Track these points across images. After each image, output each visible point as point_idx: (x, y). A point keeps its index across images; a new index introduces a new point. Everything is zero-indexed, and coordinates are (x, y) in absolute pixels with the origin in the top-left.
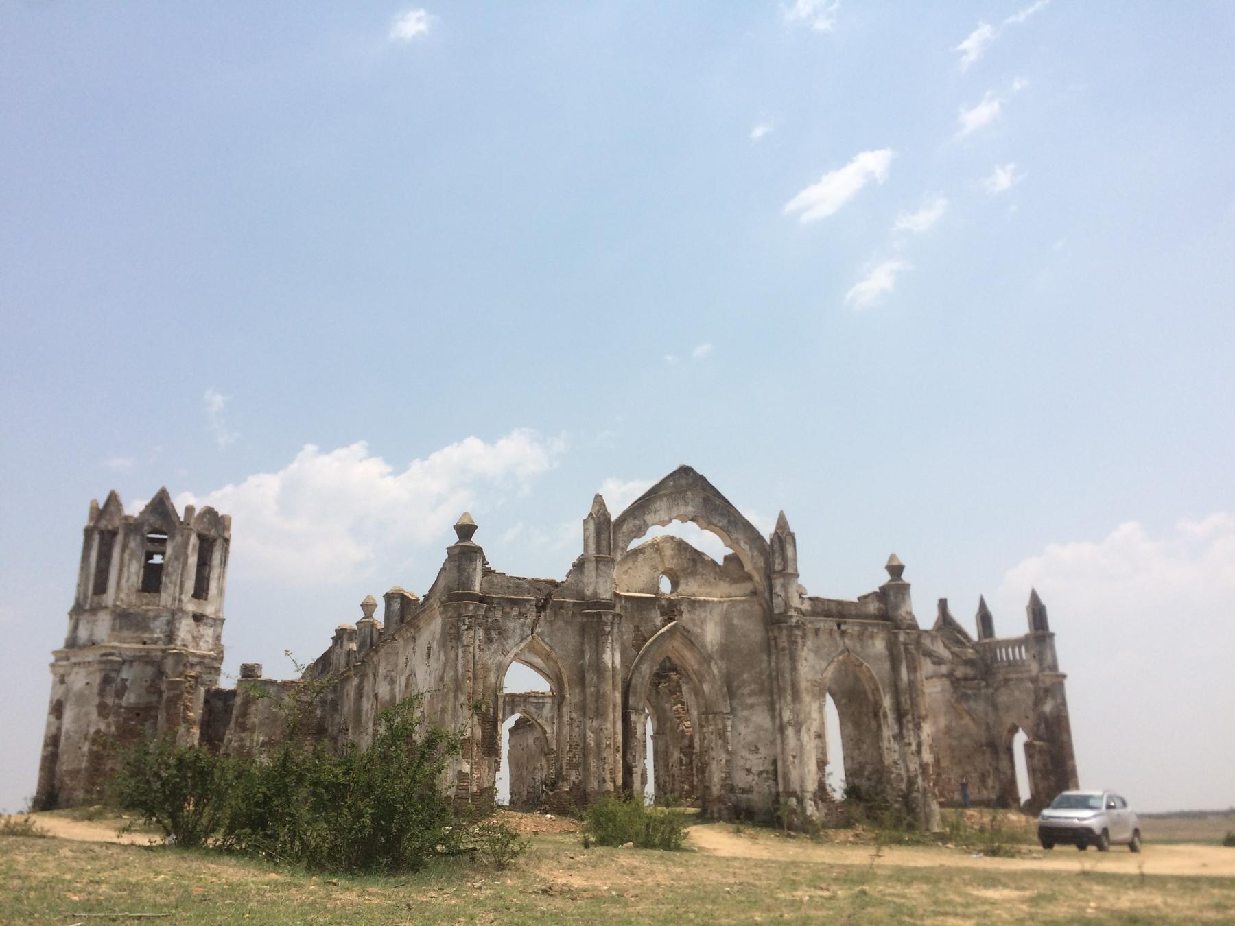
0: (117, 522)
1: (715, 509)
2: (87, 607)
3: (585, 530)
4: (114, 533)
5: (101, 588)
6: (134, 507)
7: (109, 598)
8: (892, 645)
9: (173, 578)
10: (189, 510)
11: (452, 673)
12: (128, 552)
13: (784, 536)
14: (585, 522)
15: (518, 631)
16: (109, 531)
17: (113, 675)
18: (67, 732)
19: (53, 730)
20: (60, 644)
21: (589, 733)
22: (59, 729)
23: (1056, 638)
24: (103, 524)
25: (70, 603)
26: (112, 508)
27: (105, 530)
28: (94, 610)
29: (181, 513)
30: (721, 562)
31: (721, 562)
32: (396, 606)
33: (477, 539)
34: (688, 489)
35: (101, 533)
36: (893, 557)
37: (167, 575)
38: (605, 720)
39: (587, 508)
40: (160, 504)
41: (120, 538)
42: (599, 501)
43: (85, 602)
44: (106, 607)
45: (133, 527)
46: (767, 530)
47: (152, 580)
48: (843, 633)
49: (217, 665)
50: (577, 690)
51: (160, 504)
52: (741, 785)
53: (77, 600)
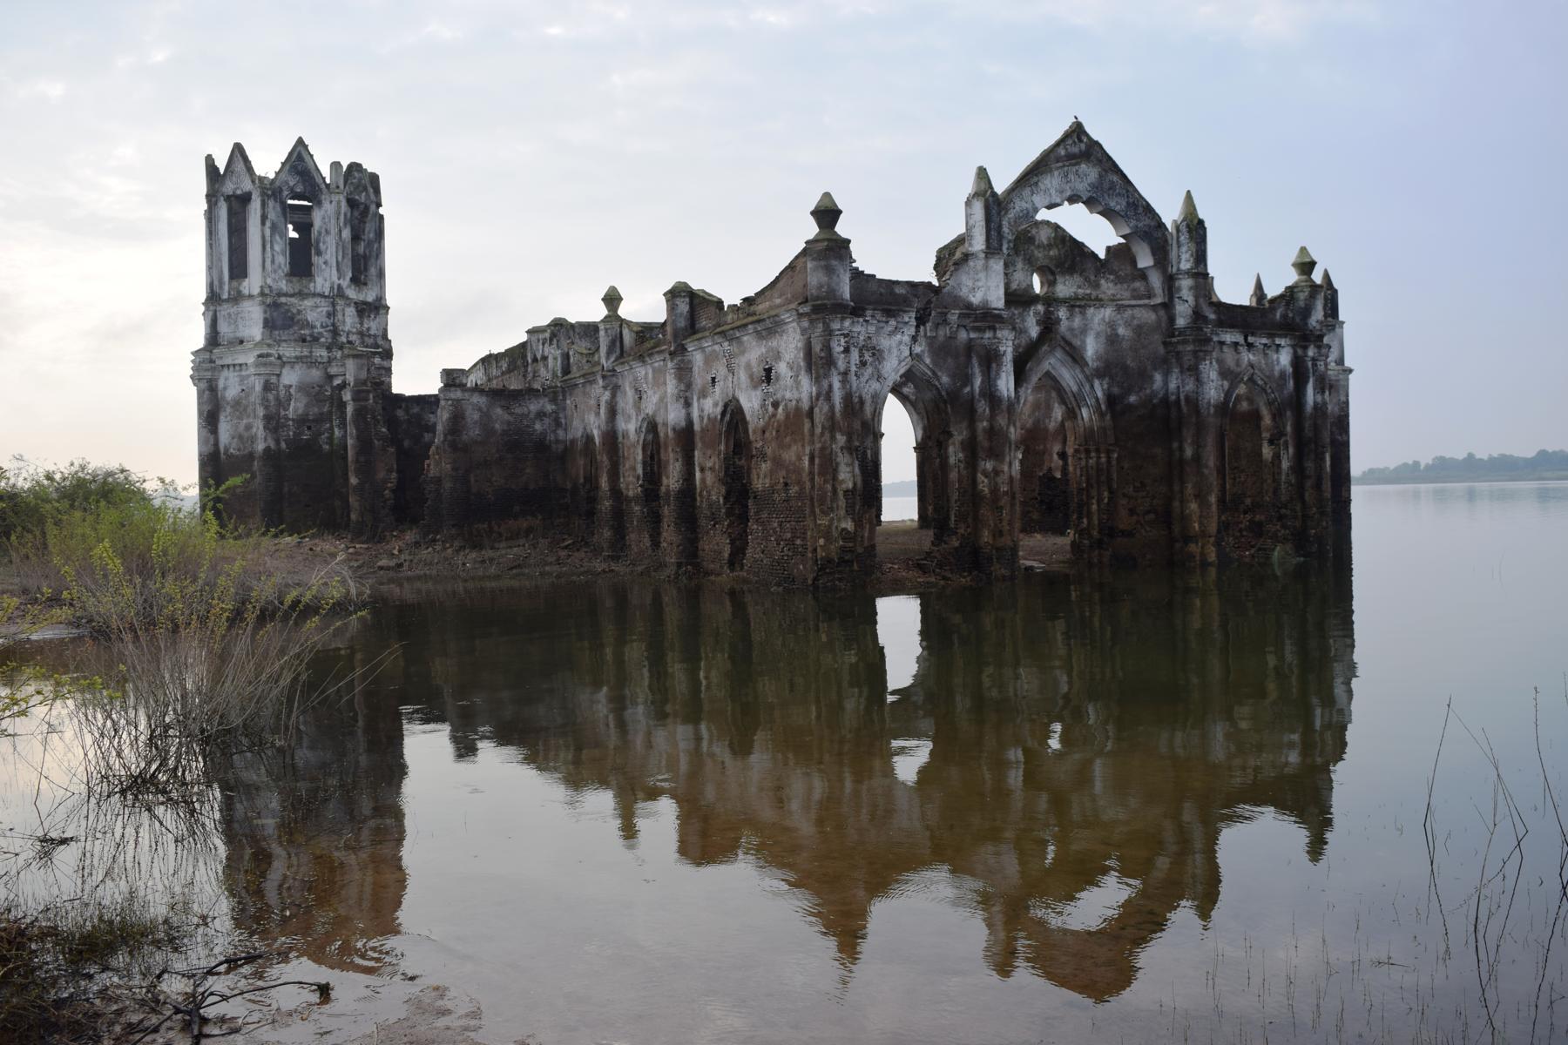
0: (247, 186)
1: (1111, 190)
2: (225, 296)
3: (968, 216)
4: (245, 199)
5: (239, 268)
6: (267, 162)
7: (253, 283)
8: (1298, 362)
9: (328, 257)
10: (336, 166)
11: (826, 408)
12: (268, 224)
13: (1195, 229)
14: (968, 203)
15: (895, 351)
16: (237, 197)
17: (274, 379)
18: (227, 450)
19: (209, 449)
20: (199, 342)
21: (980, 477)
22: (216, 444)
23: (854, 248)
24: (229, 188)
25: (202, 295)
26: (239, 166)
27: (230, 193)
28: (237, 298)
29: (326, 171)
30: (1102, 255)
31: (1102, 255)
32: (683, 306)
33: (842, 229)
34: (1078, 159)
35: (228, 198)
36: (1303, 250)
37: (319, 253)
38: (1002, 461)
39: (968, 186)
40: (299, 160)
41: (255, 207)
42: (982, 173)
43: (221, 287)
44: (251, 296)
45: (271, 190)
46: (1170, 214)
47: (301, 259)
48: (1250, 346)
49: (385, 363)
50: (965, 424)
51: (299, 160)
52: (1121, 527)
53: (211, 286)
